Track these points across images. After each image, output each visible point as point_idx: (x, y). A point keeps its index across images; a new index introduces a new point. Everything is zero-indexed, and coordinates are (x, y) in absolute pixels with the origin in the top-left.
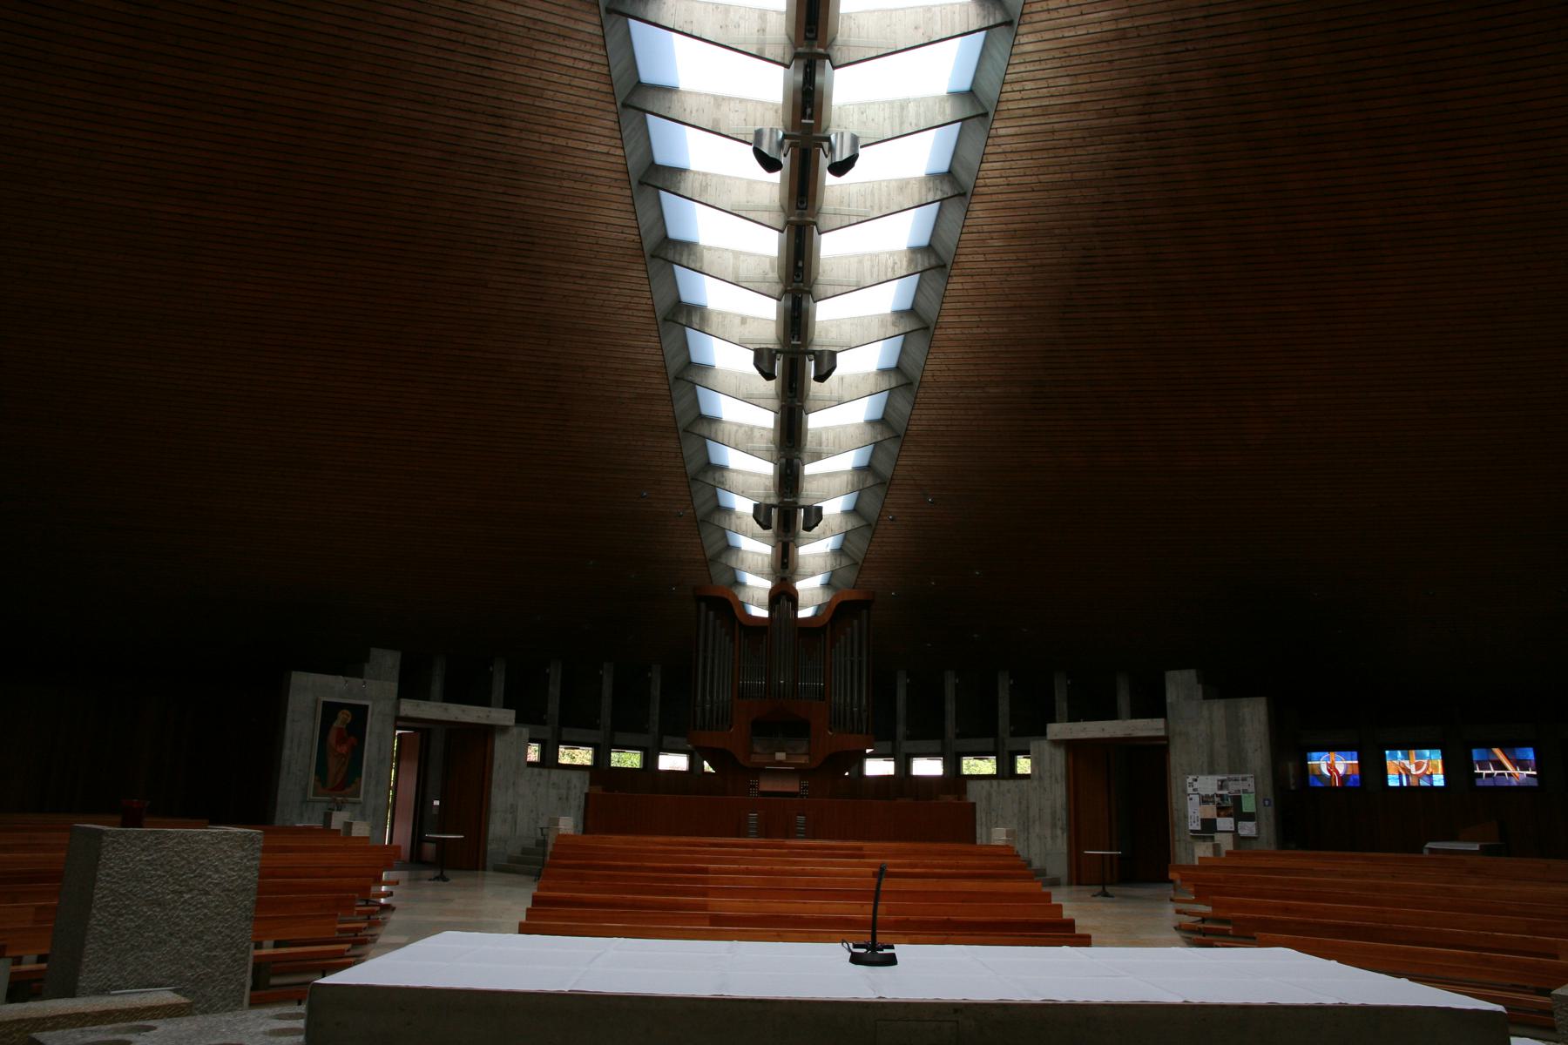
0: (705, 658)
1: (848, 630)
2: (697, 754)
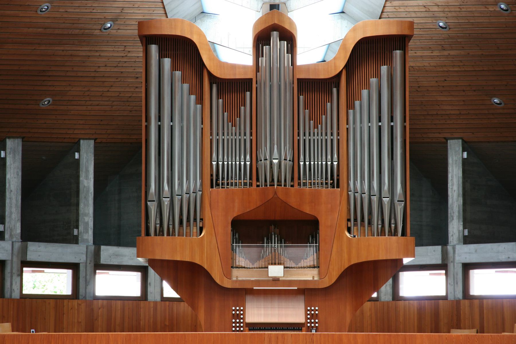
0: (160, 129)
1: (374, 81)
2: (151, 272)
